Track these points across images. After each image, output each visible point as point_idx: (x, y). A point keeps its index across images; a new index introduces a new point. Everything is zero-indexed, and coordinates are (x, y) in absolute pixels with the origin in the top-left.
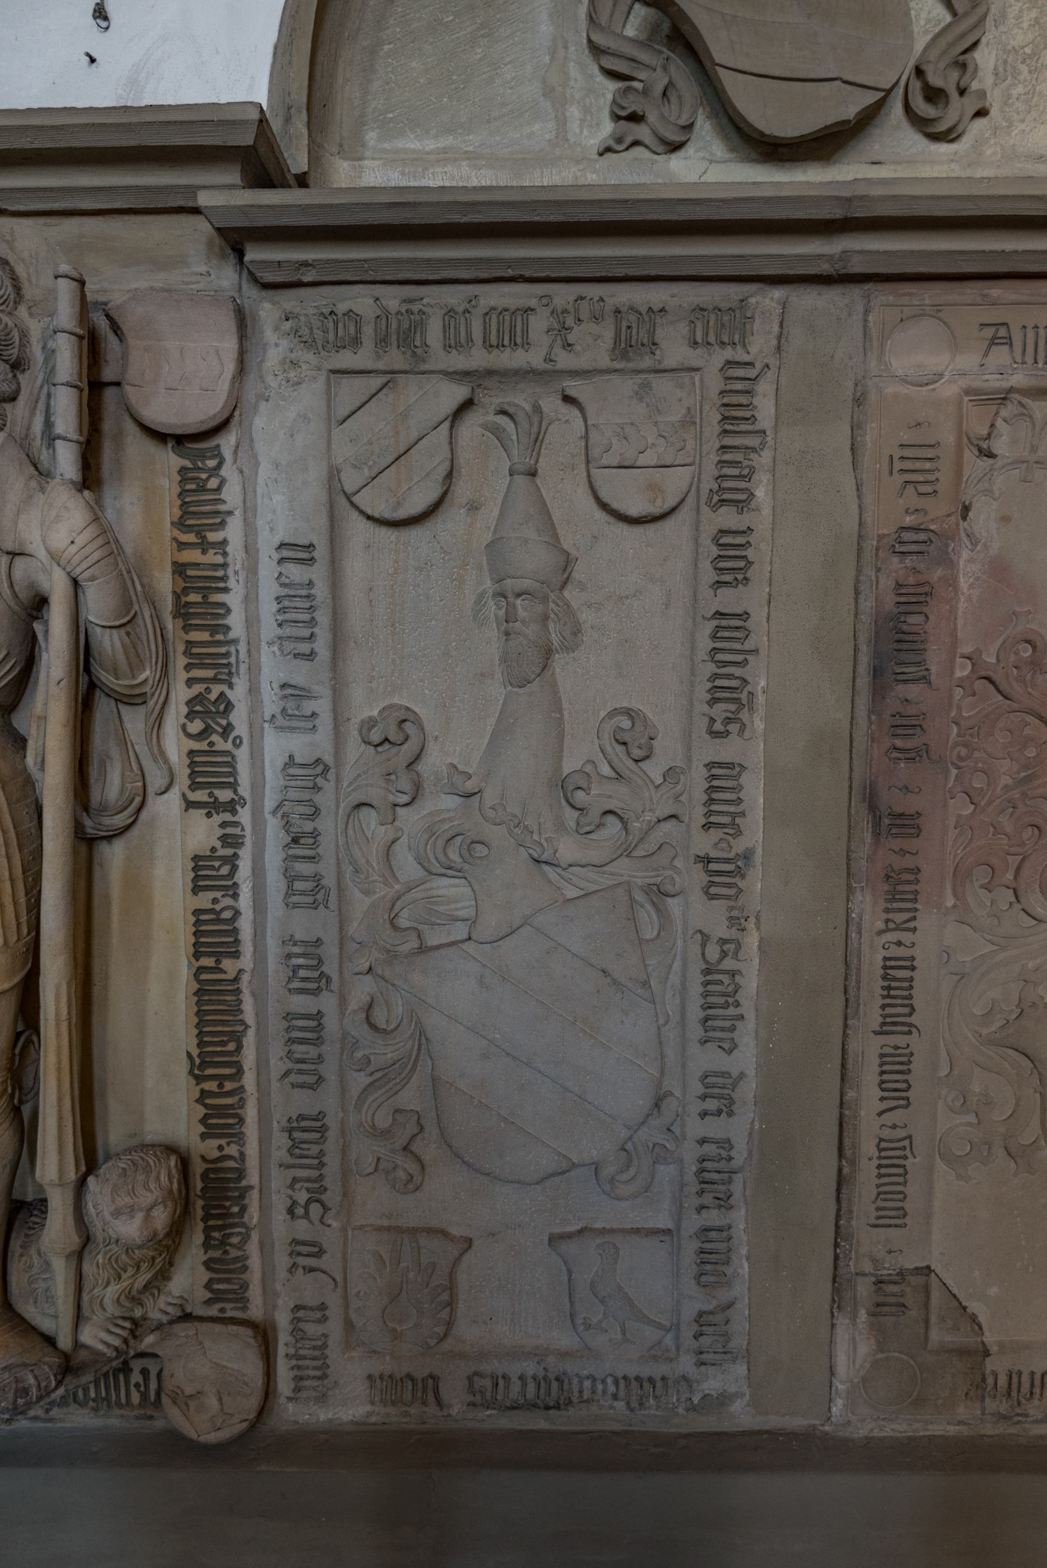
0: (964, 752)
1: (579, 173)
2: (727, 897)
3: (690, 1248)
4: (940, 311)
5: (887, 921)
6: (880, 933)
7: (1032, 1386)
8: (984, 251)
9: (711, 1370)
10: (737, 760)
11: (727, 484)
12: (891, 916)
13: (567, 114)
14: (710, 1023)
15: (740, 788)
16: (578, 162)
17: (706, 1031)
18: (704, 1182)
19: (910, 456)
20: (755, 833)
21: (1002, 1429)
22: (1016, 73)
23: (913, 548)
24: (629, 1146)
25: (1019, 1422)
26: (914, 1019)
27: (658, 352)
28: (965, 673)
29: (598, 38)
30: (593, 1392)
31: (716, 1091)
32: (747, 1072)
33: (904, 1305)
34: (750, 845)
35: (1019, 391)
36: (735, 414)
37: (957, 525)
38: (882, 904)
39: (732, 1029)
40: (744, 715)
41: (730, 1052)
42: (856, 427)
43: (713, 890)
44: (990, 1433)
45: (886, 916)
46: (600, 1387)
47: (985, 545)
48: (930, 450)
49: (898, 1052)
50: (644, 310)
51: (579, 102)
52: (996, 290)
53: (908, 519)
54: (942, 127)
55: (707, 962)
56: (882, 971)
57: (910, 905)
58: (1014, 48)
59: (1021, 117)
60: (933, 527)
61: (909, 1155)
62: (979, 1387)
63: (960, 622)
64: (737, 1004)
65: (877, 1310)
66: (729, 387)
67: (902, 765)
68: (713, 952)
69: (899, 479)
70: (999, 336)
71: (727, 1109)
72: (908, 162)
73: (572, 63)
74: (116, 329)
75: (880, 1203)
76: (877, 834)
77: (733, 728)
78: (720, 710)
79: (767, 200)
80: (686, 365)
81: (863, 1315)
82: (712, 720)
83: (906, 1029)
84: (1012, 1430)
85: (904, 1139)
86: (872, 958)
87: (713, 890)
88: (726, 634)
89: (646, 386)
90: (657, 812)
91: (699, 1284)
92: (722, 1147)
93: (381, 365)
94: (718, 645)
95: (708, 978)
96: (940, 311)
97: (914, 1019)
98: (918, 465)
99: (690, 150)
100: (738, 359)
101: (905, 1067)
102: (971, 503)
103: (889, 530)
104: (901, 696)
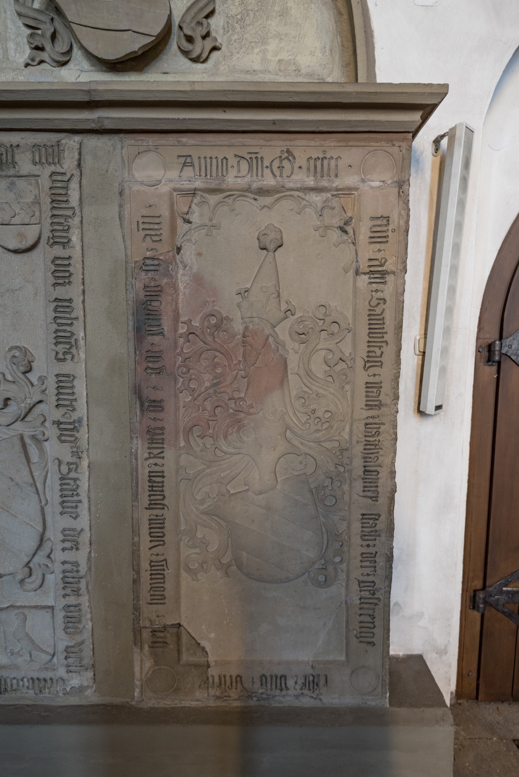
0: (185, 370)
1: (15, 77)
2: (70, 442)
3: (60, 615)
4: (157, 149)
5: (150, 453)
6: (146, 459)
7: (231, 683)
8: (169, 119)
9: (74, 675)
10: (71, 373)
11: (56, 234)
12: (151, 451)
13: (8, 46)
14: (65, 504)
15: (73, 387)
16: (14, 70)
17: (63, 508)
18: (66, 583)
19: (147, 222)
20: (82, 410)
21: (219, 703)
22: (234, 28)
23: (152, 268)
24: (31, 565)
25: (226, 700)
26: (165, 502)
27: (17, 167)
28: (184, 331)
30: (18, 686)
31: (70, 538)
32: (85, 528)
33: (166, 643)
34: (80, 415)
35: (200, 190)
36: (58, 199)
37: (174, 257)
38: (147, 445)
39: (76, 507)
40: (74, 350)
41: (75, 518)
42: (121, 206)
43: (63, 438)
44: (213, 705)
45: (149, 451)
46: (21, 683)
47: (190, 268)
48: (157, 219)
49: (158, 518)
51: (13, 40)
52: (185, 139)
53: (148, 253)
54: (194, 55)
55: (62, 474)
56: (148, 478)
57: (160, 446)
58: (232, 15)
59: (237, 51)
60: (161, 258)
61: (166, 569)
62: (206, 682)
63: (180, 305)
64: (78, 495)
65: (153, 645)
66: (54, 185)
67: (153, 376)
68: (64, 469)
69: (142, 233)
70: (187, 162)
71: (76, 547)
72: (181, 73)
73: (9, 21)
75: (152, 593)
76: (142, 410)
77: (68, 357)
78: (61, 348)
79: (48, 91)
80: (32, 174)
81: (146, 648)
82: (57, 353)
83: (162, 506)
84: (223, 704)
85: (163, 561)
86: (143, 473)
87: (63, 438)
88: (62, 310)
89: (13, 184)
90: (33, 399)
91: (66, 632)
92: (74, 566)
94: (58, 315)
95: (63, 482)
96: (157, 149)
97: (165, 502)
98: (152, 226)
99: (71, 65)
100: (58, 171)
101: (162, 526)
102: (181, 246)
103: (139, 258)
104: (150, 342)
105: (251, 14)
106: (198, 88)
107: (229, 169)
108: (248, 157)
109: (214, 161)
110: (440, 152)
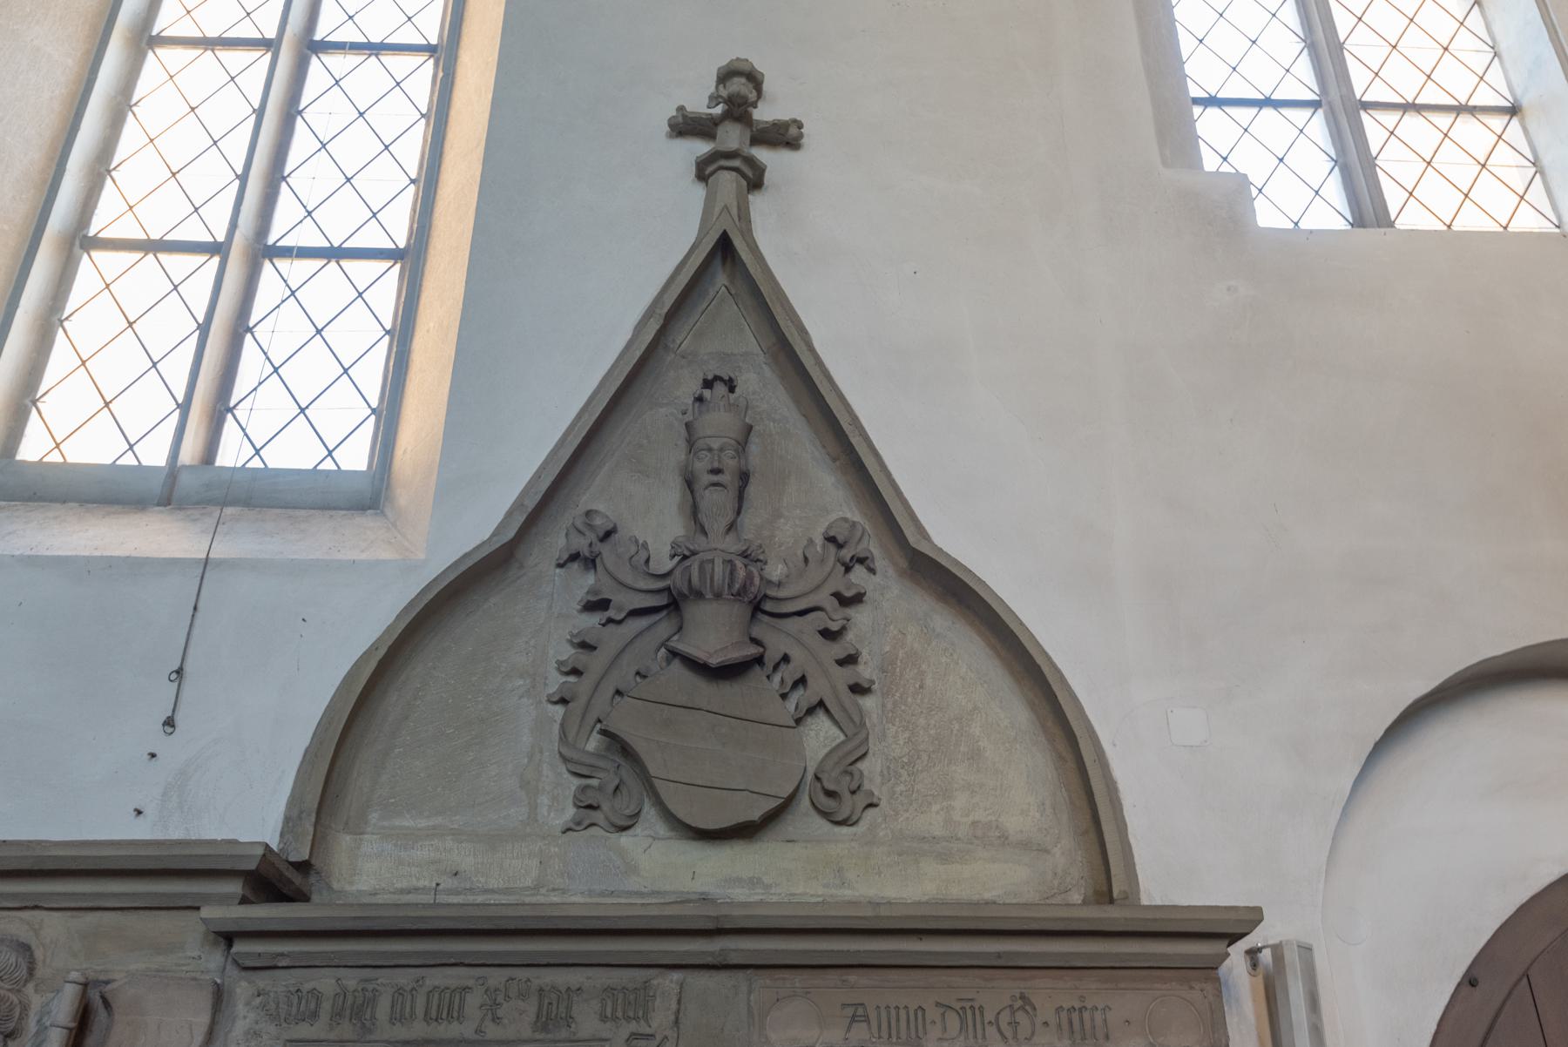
29: (565, 751)
50: (563, 990)
52: (853, 977)
74: (107, 1004)
93: (332, 1036)
99: (638, 830)
100: (641, 1031)
105: (925, 757)
106: (884, 912)
107: (928, 1026)
108: (957, 1006)
109: (903, 1013)
110: (1260, 970)
